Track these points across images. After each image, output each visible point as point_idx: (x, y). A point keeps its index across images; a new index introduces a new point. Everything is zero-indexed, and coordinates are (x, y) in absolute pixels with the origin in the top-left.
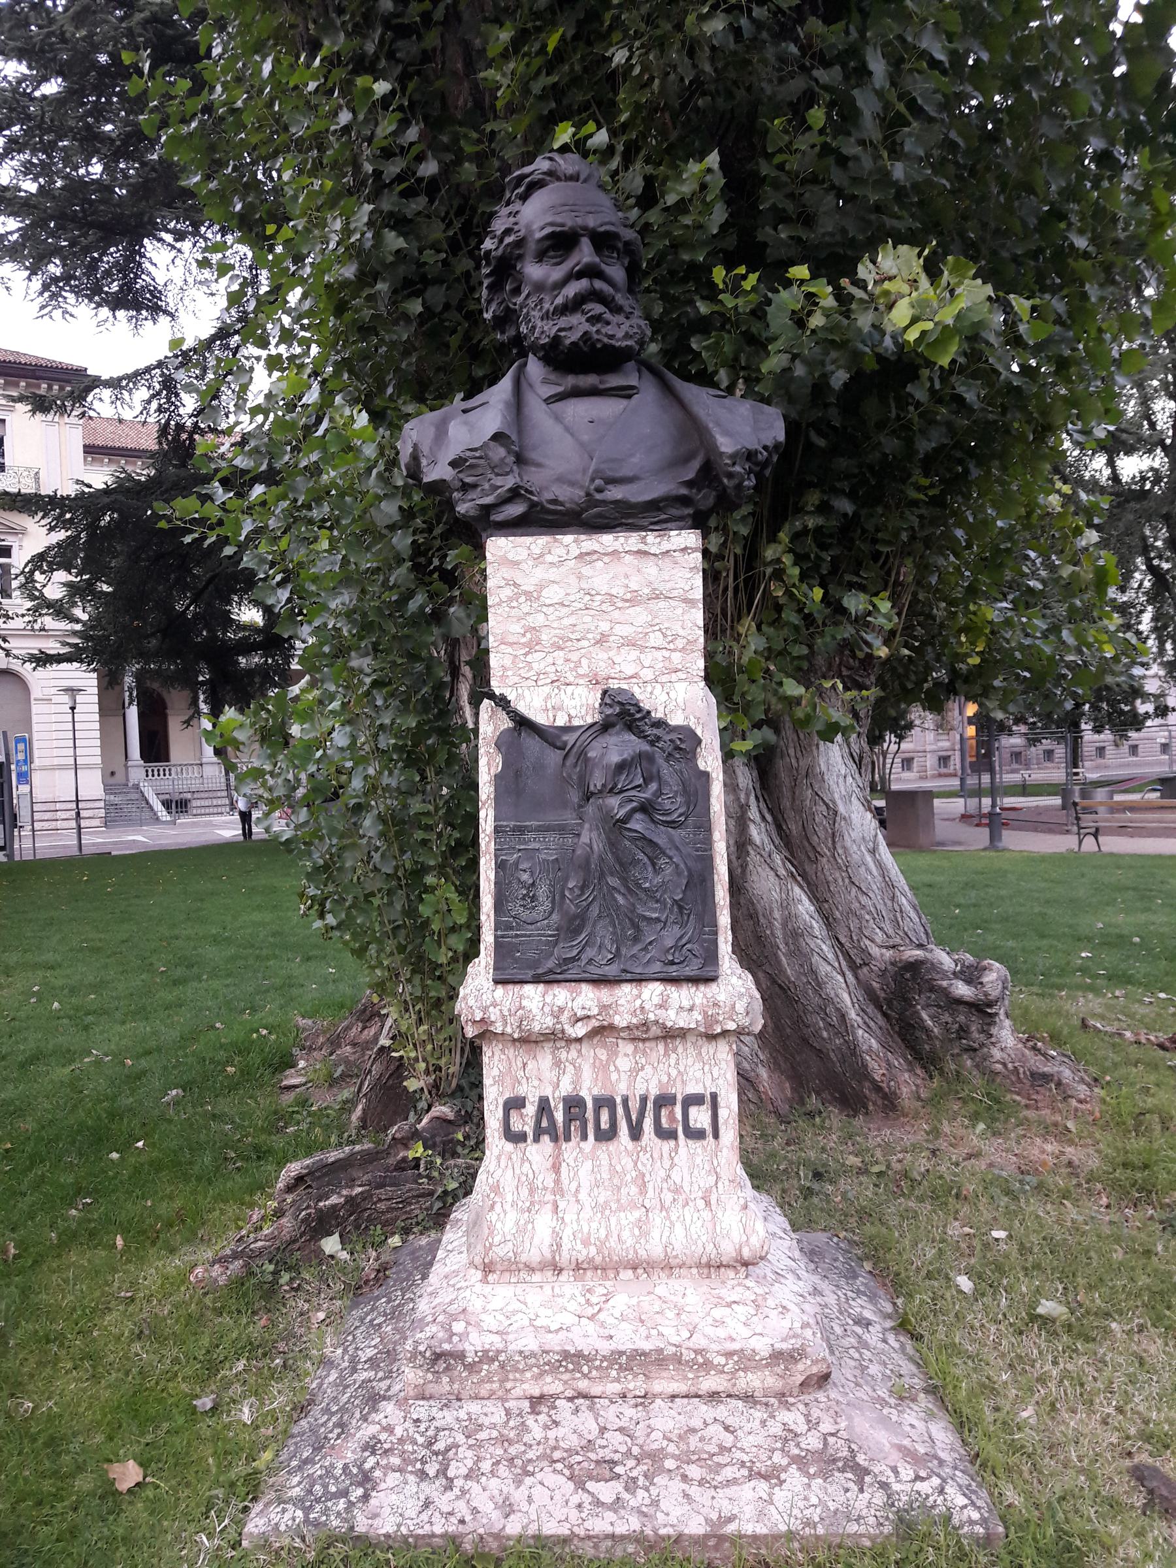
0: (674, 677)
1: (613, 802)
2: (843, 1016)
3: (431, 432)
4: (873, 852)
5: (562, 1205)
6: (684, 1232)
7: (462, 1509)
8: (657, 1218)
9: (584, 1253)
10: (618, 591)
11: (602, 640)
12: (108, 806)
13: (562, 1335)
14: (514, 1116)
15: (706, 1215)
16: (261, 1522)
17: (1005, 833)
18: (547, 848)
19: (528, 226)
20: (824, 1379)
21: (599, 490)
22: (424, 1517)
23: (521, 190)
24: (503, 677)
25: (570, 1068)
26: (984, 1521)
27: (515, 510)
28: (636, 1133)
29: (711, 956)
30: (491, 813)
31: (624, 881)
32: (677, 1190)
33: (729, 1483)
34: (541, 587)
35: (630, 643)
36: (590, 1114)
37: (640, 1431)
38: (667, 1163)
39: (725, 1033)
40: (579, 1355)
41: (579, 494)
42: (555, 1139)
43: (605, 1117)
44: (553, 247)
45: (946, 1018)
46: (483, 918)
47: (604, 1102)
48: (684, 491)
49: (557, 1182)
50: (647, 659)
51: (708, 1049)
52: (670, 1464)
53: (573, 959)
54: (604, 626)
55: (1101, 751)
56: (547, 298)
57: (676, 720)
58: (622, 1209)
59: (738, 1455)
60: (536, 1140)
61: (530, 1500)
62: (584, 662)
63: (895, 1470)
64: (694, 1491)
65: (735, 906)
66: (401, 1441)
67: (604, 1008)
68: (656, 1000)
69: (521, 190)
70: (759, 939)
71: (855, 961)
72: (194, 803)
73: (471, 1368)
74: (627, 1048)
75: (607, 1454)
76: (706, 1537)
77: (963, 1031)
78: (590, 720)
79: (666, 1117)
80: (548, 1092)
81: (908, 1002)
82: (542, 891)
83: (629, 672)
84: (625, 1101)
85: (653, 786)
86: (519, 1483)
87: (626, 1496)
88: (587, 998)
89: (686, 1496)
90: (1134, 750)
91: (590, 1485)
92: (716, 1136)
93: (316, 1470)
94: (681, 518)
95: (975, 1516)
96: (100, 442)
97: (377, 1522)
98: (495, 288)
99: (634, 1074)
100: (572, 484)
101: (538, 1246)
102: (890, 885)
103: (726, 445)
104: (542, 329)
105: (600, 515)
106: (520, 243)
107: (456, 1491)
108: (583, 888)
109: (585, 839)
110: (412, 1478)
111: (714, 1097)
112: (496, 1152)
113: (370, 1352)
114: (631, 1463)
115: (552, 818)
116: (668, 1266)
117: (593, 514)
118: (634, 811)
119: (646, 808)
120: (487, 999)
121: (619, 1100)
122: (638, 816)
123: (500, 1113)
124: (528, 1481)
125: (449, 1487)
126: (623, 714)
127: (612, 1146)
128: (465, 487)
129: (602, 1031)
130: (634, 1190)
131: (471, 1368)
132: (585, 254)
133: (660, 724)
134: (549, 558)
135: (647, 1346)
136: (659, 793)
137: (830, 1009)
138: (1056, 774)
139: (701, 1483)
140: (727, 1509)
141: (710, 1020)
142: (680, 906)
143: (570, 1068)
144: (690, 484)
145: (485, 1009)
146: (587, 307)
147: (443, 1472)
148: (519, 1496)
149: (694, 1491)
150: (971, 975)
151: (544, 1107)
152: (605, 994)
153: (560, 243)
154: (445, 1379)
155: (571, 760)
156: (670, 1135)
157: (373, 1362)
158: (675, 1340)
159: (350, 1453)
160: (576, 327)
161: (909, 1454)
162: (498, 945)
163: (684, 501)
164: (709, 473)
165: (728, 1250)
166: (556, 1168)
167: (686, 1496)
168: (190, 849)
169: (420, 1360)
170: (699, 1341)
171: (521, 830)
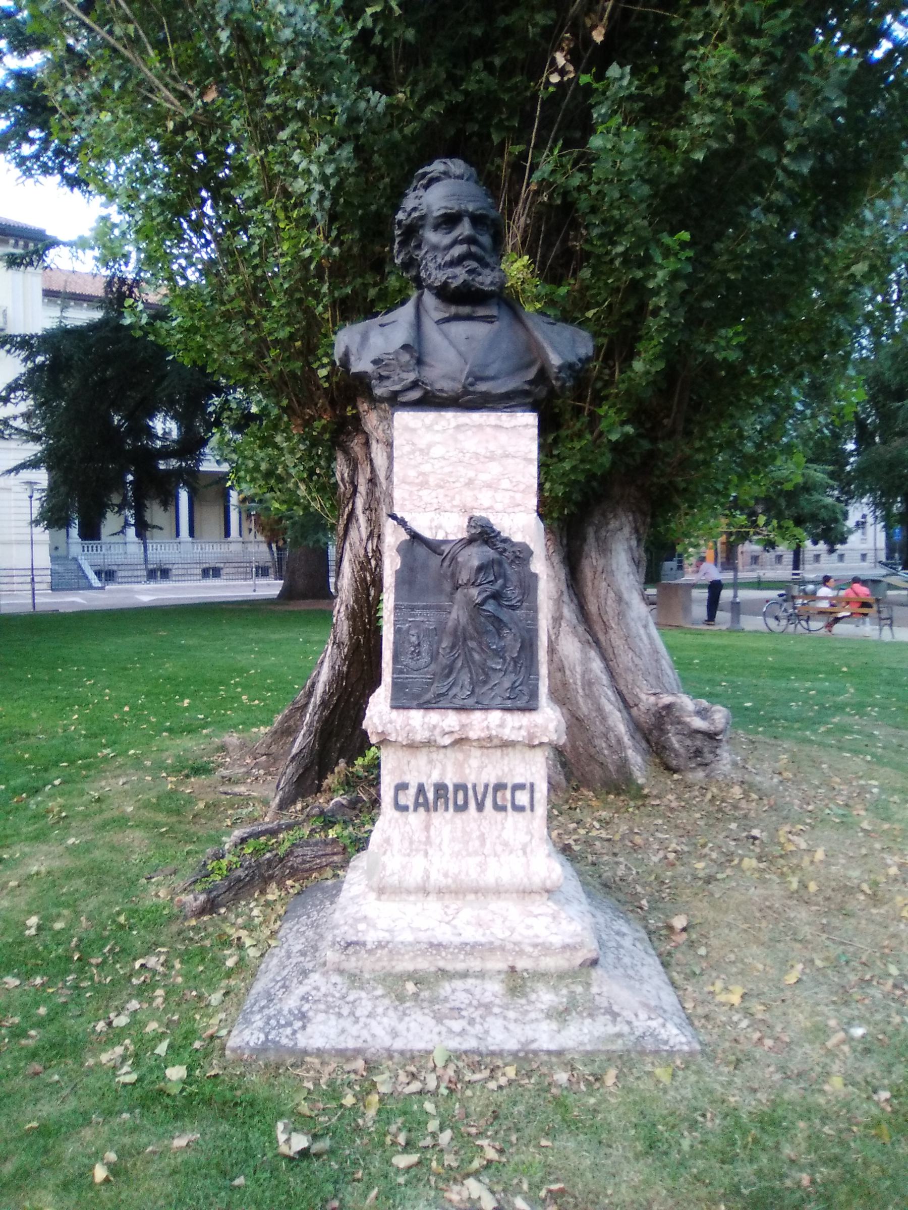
0: (517, 509)
1: (474, 591)
2: (619, 741)
3: (357, 338)
4: (645, 627)
5: (430, 852)
6: (506, 869)
7: (365, 1034)
8: (492, 861)
9: (443, 882)
10: (482, 451)
11: (470, 483)
12: (53, 573)
13: (429, 933)
14: (401, 794)
15: (523, 860)
16: (238, 1040)
17: (743, 618)
18: (429, 620)
19: (429, 207)
20: (594, 963)
21: (472, 385)
22: (342, 1038)
23: (424, 182)
24: (403, 506)
25: (439, 765)
26: (689, 1043)
27: (415, 395)
28: (480, 807)
29: (534, 695)
30: (392, 596)
31: (480, 643)
32: (506, 844)
33: (532, 1021)
34: (430, 446)
35: (489, 486)
36: (451, 795)
37: (477, 992)
38: (499, 827)
39: (541, 744)
40: (440, 945)
41: (458, 387)
42: (427, 810)
43: (461, 795)
44: (445, 222)
45: (688, 742)
46: (384, 665)
47: (460, 787)
48: (527, 387)
49: (428, 837)
50: (499, 496)
51: (529, 754)
52: (496, 1010)
53: (443, 695)
54: (471, 474)
55: (817, 557)
56: (440, 255)
57: (517, 538)
58: (469, 855)
59: (539, 1005)
60: (415, 810)
61: (408, 1030)
62: (458, 497)
63: (636, 1015)
64: (512, 1026)
65: (551, 661)
66: (325, 995)
67: (463, 726)
68: (498, 722)
69: (424, 182)
70: (565, 684)
71: (626, 704)
72: (120, 574)
73: (370, 952)
74: (476, 753)
75: (457, 1004)
76: (518, 1051)
77: (698, 753)
78: (460, 537)
79: (500, 797)
80: (423, 780)
81: (663, 732)
82: (425, 647)
83: (487, 504)
84: (474, 786)
85: (500, 582)
86: (401, 1020)
87: (468, 1028)
88: (450, 720)
89: (506, 1028)
90: (841, 557)
91: (446, 1022)
92: (532, 809)
93: (271, 1011)
94: (523, 405)
95: (684, 1040)
96: (55, 288)
97: (311, 1041)
98: (404, 244)
99: (481, 770)
100: (453, 379)
101: (414, 877)
102: (656, 652)
103: (555, 360)
104: (438, 277)
105: (470, 401)
106: (422, 218)
107: (361, 1024)
108: (453, 647)
109: (454, 615)
110: (333, 1017)
111: (532, 785)
112: (388, 817)
113: (299, 947)
114: (472, 1010)
115: (432, 601)
116: (498, 891)
117: (467, 400)
118: (487, 598)
119: (496, 596)
120: (386, 718)
121: (470, 786)
122: (491, 601)
123: (392, 793)
124: (407, 1019)
125: (357, 1021)
126: (483, 534)
127: (464, 816)
128: (381, 378)
129: (460, 742)
130: (477, 843)
131: (370, 952)
132: (465, 229)
133: (506, 540)
134: (436, 427)
135: (483, 940)
136: (504, 586)
137: (611, 735)
138: (784, 572)
139: (516, 1021)
140: (530, 1035)
141: (531, 736)
142: (515, 661)
143: (439, 765)
144: (530, 382)
145: (385, 725)
146: (466, 263)
147: (352, 1013)
148: (401, 1027)
149: (512, 1026)
150: (702, 713)
151: (421, 789)
152: (464, 717)
153: (449, 221)
154: (353, 959)
155: (446, 563)
156: (503, 809)
157: (303, 953)
158: (501, 936)
159: (292, 1002)
160: (460, 275)
161: (646, 1006)
162: (395, 684)
163: (526, 393)
164: (542, 375)
165: (537, 881)
166: (427, 828)
167: (506, 1028)
168: (129, 609)
169: (337, 947)
170: (516, 937)
171: (413, 608)
